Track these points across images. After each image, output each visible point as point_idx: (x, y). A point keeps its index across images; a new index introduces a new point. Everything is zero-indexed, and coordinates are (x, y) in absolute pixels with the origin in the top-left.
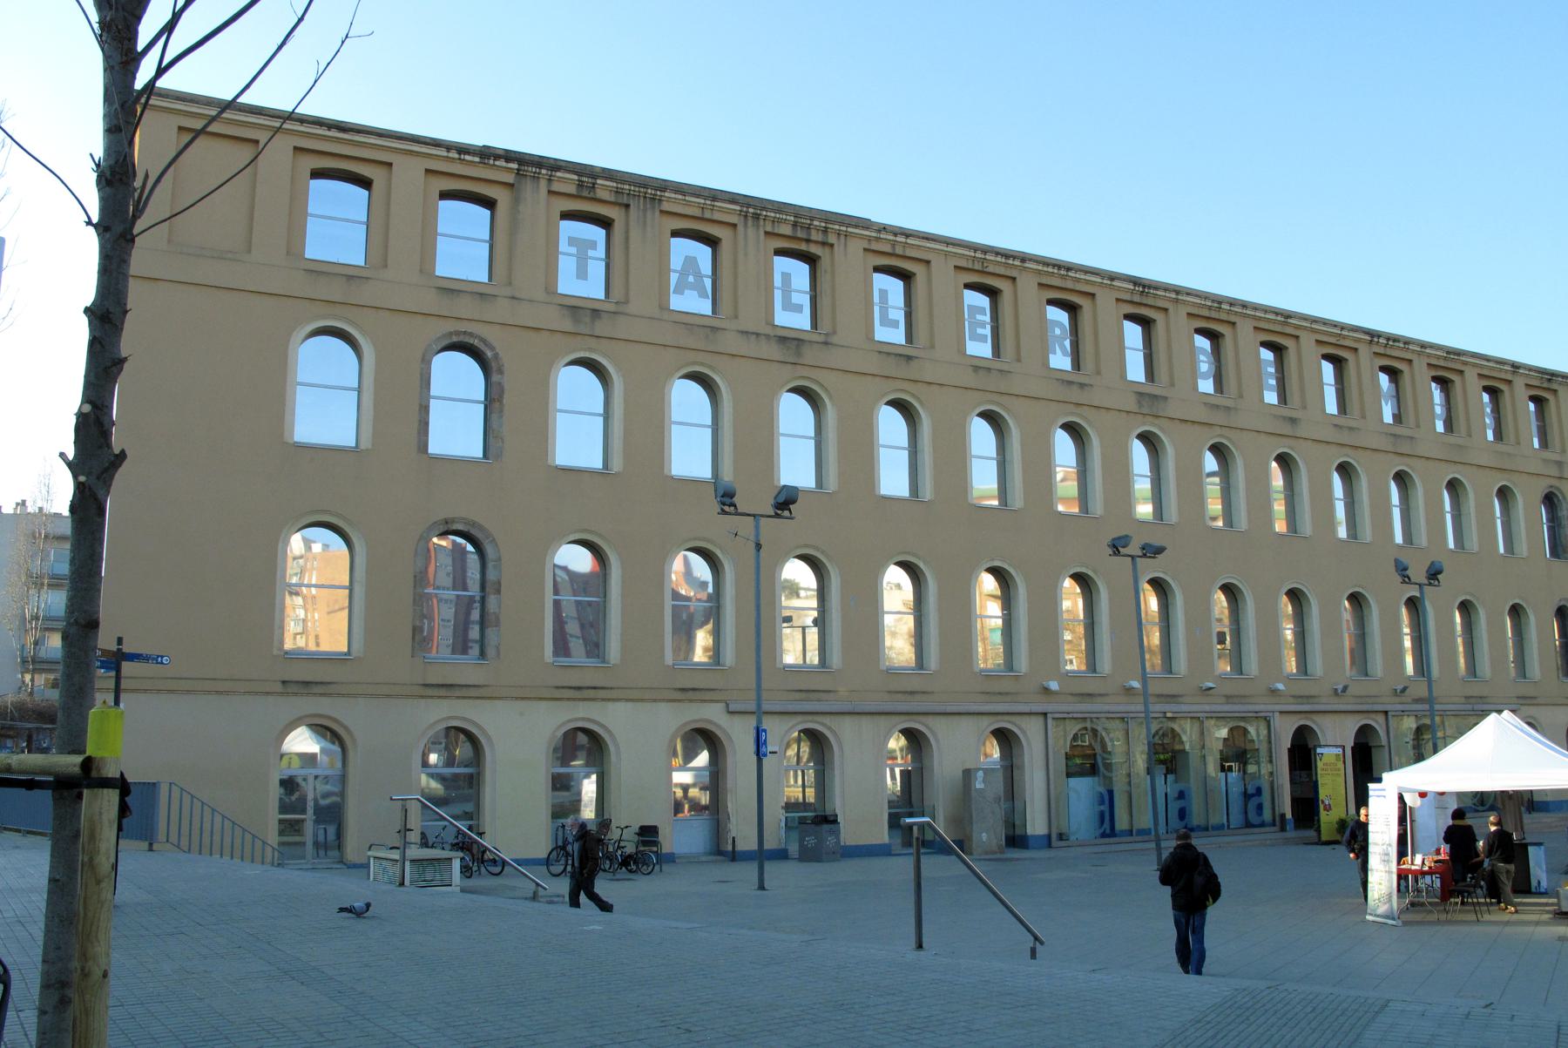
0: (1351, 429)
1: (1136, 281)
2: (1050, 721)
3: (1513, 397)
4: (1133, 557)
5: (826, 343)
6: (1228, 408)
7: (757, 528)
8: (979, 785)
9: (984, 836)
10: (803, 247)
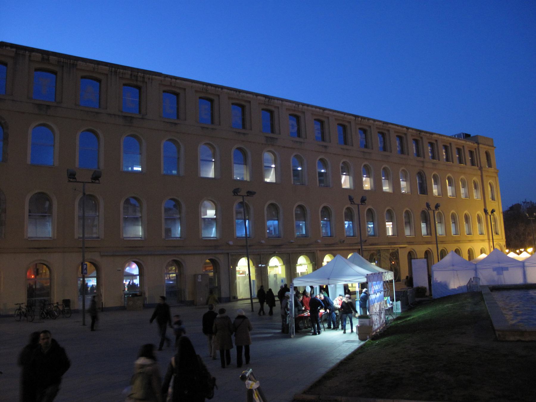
0: (347, 149)
1: (266, 96)
2: (230, 256)
3: (422, 142)
4: (243, 196)
5: (142, 118)
6: (301, 142)
7: (84, 186)
8: (200, 280)
9: (201, 299)
10: (173, 89)
